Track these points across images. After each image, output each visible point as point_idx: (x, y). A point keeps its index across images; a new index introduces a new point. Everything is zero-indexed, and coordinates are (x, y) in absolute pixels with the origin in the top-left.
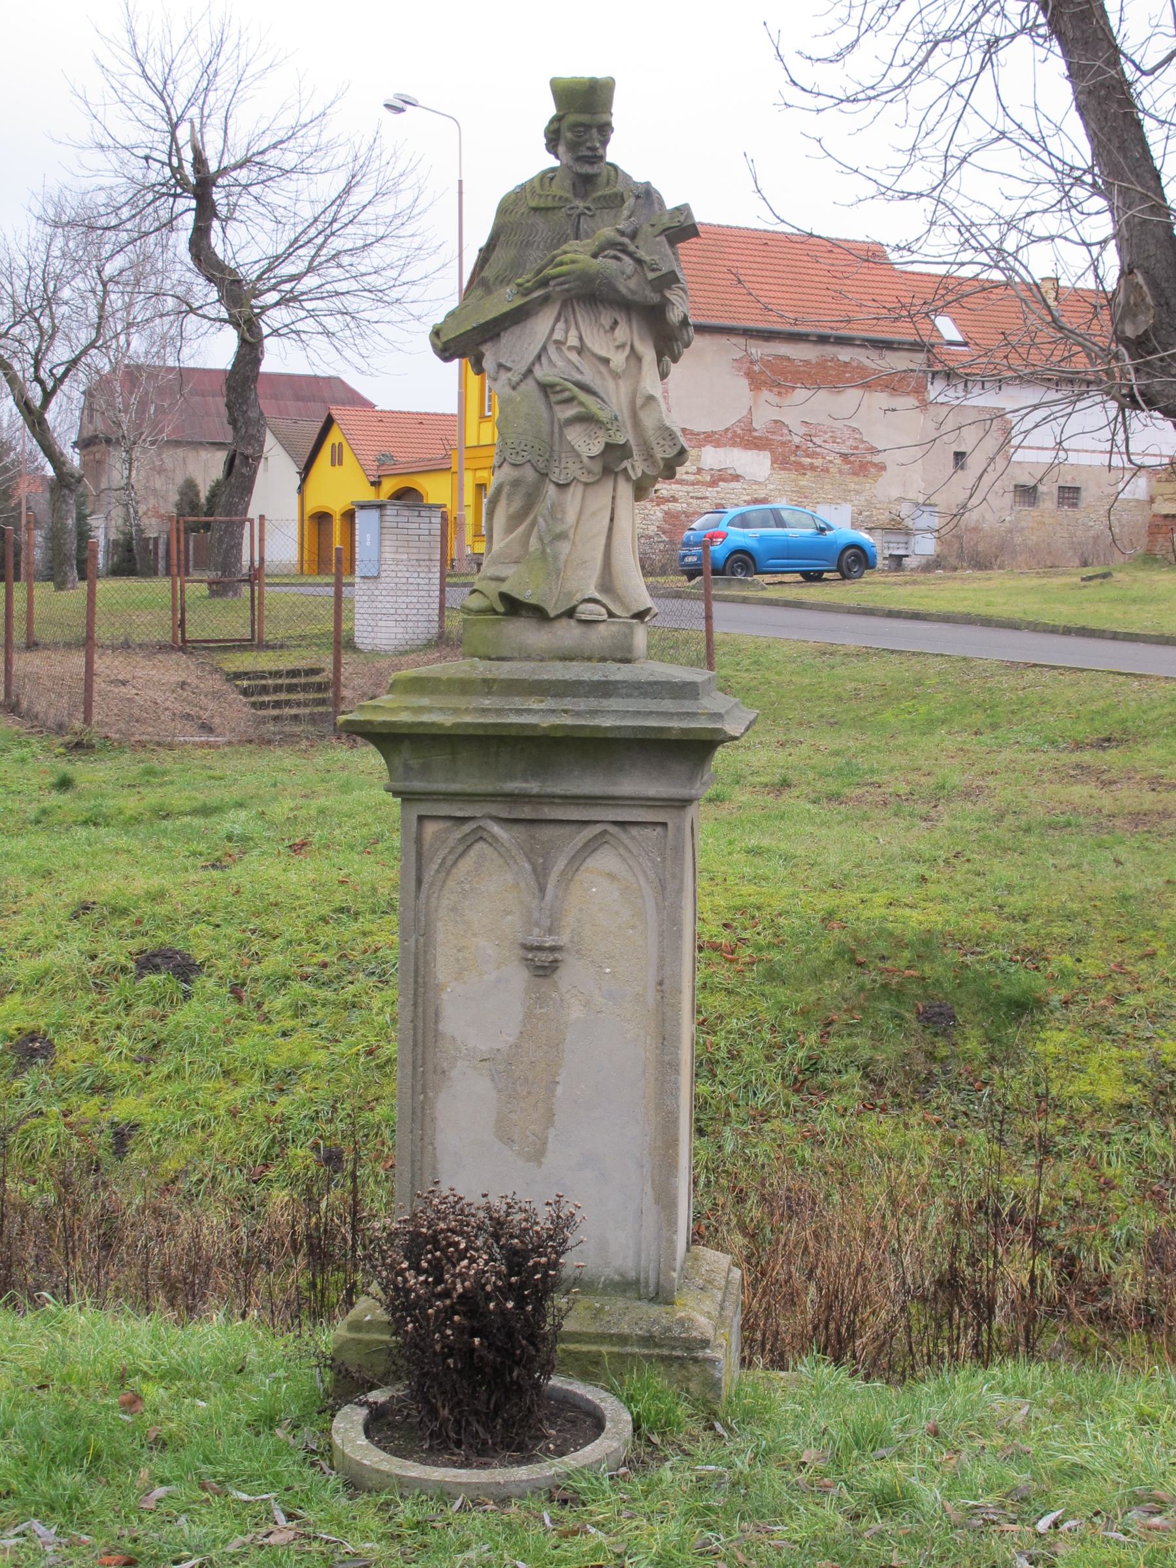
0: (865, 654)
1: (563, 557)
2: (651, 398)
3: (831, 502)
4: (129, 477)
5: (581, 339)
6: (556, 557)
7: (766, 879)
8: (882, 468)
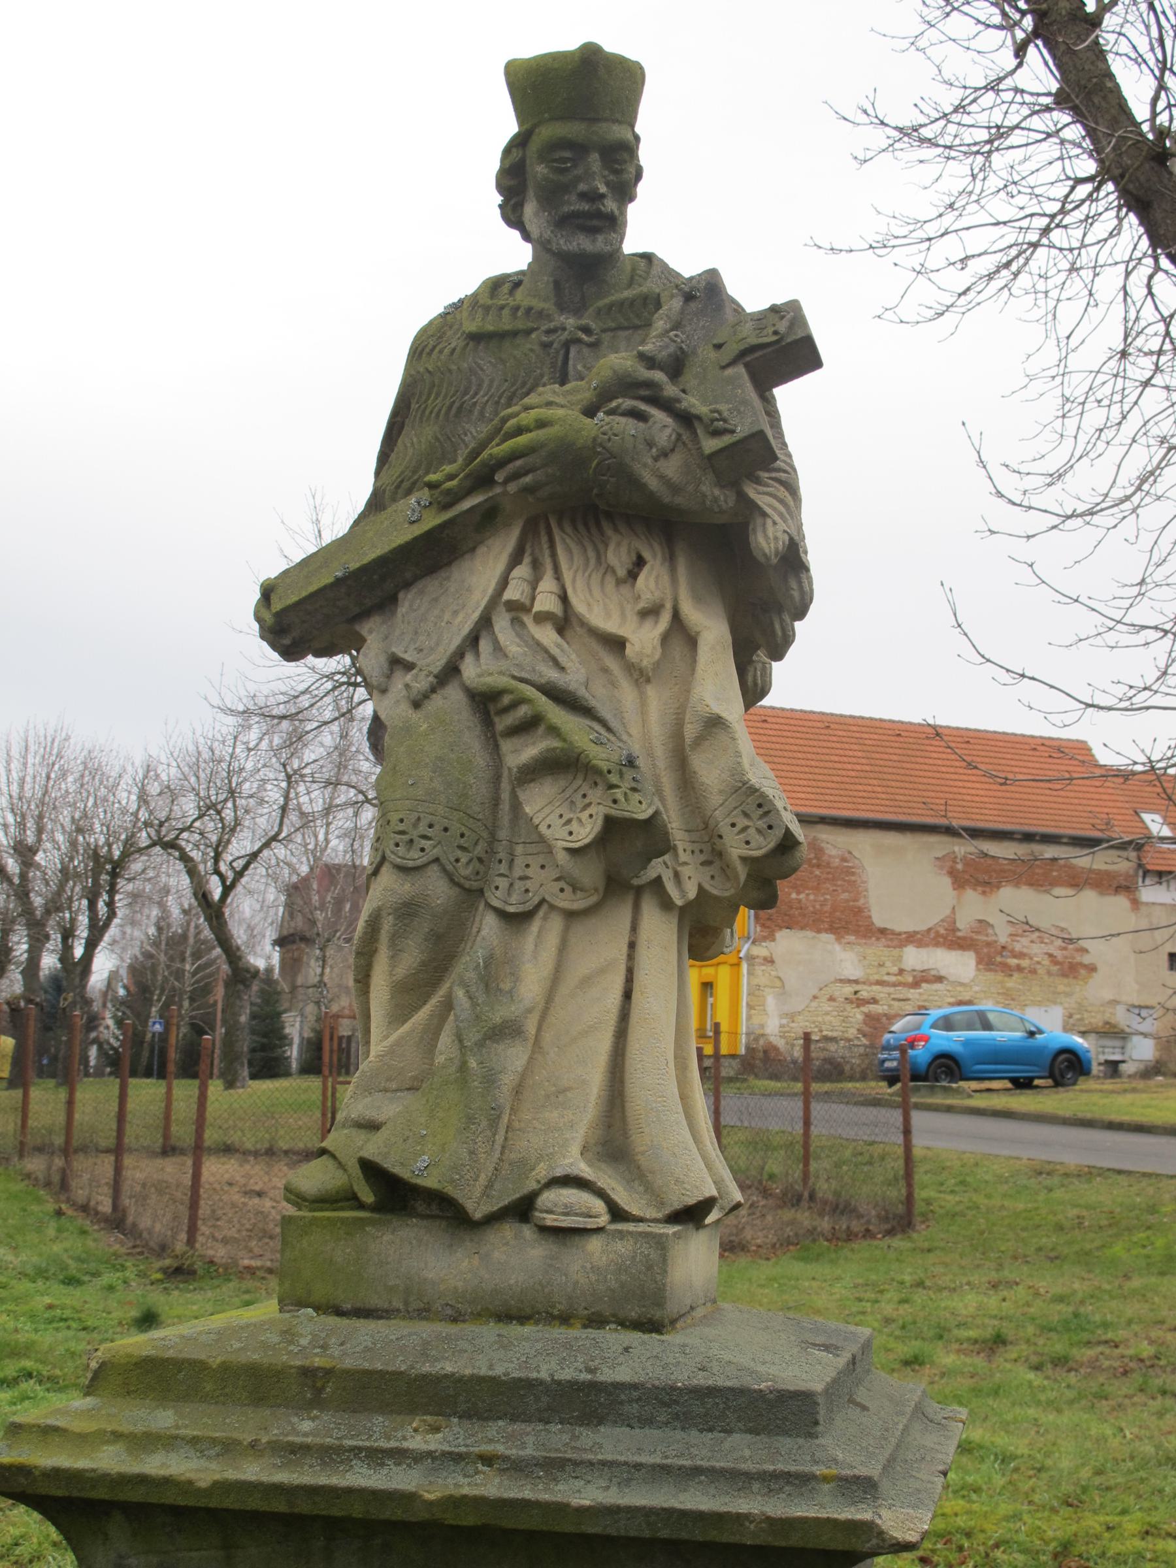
0: (1089, 1174)
1: (508, 1080)
2: (715, 723)
3: (1039, 1004)
4: (322, 974)
5: (564, 599)
6: (490, 1080)
7: (977, 1490)
8: (1092, 969)
